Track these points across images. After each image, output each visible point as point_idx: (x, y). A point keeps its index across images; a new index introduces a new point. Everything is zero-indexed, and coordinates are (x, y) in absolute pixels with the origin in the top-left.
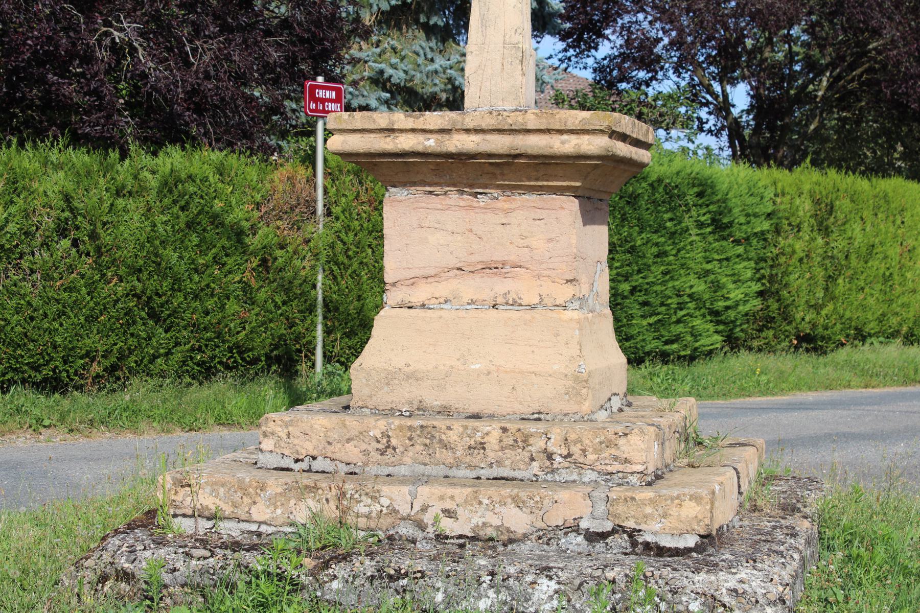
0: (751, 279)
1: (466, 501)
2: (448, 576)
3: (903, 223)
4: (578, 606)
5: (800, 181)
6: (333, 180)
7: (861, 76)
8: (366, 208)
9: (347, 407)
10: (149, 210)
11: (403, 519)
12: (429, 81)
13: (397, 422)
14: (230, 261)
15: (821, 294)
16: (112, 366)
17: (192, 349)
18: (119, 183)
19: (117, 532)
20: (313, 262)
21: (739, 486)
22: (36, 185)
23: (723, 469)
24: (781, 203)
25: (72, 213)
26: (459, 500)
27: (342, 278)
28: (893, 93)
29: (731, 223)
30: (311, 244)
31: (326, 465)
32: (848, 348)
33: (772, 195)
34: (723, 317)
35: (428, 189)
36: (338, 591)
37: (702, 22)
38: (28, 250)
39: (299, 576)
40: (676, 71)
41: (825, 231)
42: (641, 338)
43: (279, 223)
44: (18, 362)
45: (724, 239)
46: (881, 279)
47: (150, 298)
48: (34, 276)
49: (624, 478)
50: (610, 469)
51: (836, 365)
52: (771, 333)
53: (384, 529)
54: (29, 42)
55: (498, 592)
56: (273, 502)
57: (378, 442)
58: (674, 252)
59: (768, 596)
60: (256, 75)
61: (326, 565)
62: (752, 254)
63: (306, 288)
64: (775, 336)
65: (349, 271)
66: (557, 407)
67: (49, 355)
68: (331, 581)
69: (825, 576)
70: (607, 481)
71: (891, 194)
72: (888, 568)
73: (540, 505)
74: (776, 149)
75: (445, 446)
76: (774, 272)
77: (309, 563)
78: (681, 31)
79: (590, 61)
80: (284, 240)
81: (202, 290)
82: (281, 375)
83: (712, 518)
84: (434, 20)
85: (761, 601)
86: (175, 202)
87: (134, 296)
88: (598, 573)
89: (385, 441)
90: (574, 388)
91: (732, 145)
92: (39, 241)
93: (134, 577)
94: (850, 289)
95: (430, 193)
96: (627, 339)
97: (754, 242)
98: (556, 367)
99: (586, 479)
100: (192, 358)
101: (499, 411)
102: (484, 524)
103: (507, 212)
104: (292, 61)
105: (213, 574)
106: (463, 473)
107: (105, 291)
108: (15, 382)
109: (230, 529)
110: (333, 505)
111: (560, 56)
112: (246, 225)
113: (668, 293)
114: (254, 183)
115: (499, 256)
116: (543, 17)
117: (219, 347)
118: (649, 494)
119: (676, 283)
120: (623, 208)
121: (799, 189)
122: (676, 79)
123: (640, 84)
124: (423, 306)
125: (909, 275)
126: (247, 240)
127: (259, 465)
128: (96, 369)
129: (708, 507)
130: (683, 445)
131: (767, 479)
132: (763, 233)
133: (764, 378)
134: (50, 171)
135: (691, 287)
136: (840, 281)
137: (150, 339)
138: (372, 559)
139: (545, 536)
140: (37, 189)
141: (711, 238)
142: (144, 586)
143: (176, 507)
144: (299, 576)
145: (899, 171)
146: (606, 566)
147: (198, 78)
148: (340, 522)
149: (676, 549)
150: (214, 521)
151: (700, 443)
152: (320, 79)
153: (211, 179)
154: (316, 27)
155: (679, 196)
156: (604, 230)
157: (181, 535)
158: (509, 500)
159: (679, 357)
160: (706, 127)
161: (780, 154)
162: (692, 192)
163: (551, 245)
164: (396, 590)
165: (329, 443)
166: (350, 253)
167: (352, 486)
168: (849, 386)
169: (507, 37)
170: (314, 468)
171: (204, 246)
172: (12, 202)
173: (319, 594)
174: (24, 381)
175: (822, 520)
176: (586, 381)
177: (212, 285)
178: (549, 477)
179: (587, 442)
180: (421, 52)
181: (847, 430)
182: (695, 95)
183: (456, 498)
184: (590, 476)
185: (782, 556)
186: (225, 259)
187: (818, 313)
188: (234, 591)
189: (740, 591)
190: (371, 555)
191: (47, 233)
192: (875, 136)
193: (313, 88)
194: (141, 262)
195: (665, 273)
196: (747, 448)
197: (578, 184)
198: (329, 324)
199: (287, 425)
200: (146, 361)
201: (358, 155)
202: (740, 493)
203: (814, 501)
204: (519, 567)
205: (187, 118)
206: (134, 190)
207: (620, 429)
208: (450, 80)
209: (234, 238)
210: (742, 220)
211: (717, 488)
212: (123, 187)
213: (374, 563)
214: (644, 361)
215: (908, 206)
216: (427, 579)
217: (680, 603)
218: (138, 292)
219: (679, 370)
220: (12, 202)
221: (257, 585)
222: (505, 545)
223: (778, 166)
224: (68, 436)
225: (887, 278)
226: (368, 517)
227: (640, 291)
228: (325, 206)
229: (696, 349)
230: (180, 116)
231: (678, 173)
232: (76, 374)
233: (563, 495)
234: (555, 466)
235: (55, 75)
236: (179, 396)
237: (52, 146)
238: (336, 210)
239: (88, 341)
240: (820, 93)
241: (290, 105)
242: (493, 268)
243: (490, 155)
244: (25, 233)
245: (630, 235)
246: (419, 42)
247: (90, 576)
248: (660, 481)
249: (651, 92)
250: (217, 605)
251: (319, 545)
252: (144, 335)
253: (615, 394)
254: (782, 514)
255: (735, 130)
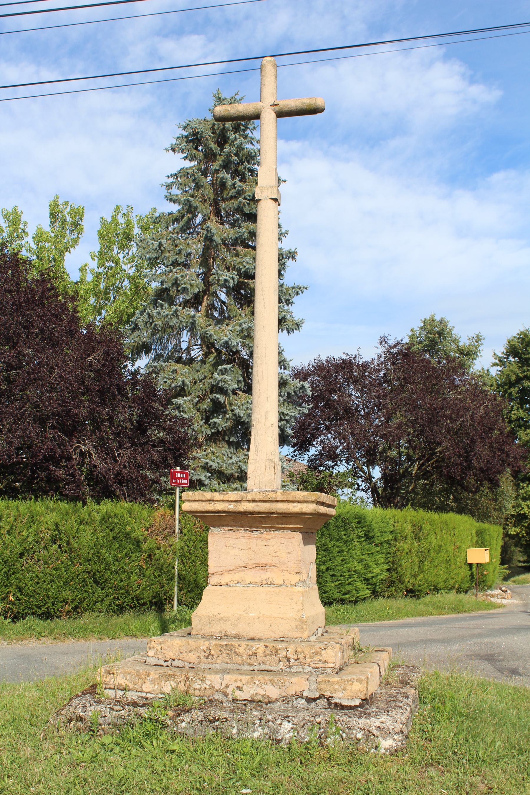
0: (384, 563)
1: (247, 682)
2: (239, 721)
3: (454, 534)
4: (302, 735)
5: (406, 515)
6: (183, 516)
7: (433, 464)
8: (199, 530)
9: (190, 634)
10: (95, 531)
11: (217, 691)
12: (229, 468)
13: (214, 642)
14: (133, 556)
15: (417, 570)
16: (75, 606)
17: (114, 598)
18: (81, 518)
19: (77, 696)
20: (173, 556)
21: (380, 673)
22: (42, 519)
23: (372, 664)
24: (397, 526)
25: (59, 532)
26: (244, 682)
27: (187, 563)
28: (448, 472)
29: (374, 536)
30: (173, 547)
31: (180, 664)
32: (430, 595)
33: (393, 522)
34: (371, 582)
35: (230, 528)
36: (185, 728)
37: (358, 439)
38: (37, 550)
39: (166, 720)
40: (347, 462)
41: (417, 538)
42: (331, 592)
43: (157, 537)
44: (30, 604)
45: (370, 543)
46: (445, 562)
47: (95, 573)
48: (40, 562)
49: (324, 670)
50: (317, 666)
51: (425, 604)
52: (393, 589)
53: (208, 696)
54: (42, 451)
55: (263, 729)
56: (153, 682)
57: (205, 652)
58: (347, 550)
59: (395, 729)
60: (148, 466)
61: (179, 715)
62: (384, 551)
63: (170, 568)
64: (396, 590)
65: (191, 560)
66: (292, 634)
67: (45, 601)
68: (181, 722)
69: (422, 718)
70: (316, 672)
71: (448, 521)
72: (452, 713)
73: (283, 684)
74: (394, 498)
75: (237, 654)
76: (394, 559)
77: (171, 713)
78: (348, 443)
79: (306, 457)
80: (160, 545)
81: (120, 569)
82: (157, 611)
83: (367, 690)
84: (232, 439)
85: (391, 732)
86: (108, 527)
87: (87, 572)
88: (312, 719)
89: (208, 652)
90: (300, 625)
91: (373, 496)
92: (43, 545)
93: (85, 720)
94: (430, 567)
95: (231, 530)
96: (325, 593)
97: (385, 545)
98: (291, 615)
99: (306, 671)
100: (114, 603)
101: (263, 636)
102: (256, 694)
103: (267, 540)
104: (165, 459)
105: (124, 719)
106: (246, 667)
107: (73, 570)
108: (29, 614)
109: (132, 696)
110: (182, 684)
111: (292, 454)
112: (141, 538)
113: (344, 570)
114: (145, 518)
115: (263, 561)
116: (284, 437)
117: (127, 597)
118: (336, 679)
119: (348, 565)
120: (322, 529)
121: (405, 519)
122: (347, 465)
123: (330, 468)
124: (227, 585)
125: (458, 559)
126: (142, 545)
127: (147, 663)
128: (67, 608)
129: (365, 685)
130: (353, 652)
131: (394, 667)
132: (389, 540)
133: (391, 611)
134: (49, 512)
135: (355, 567)
136: (426, 563)
137: (94, 593)
138: (202, 712)
139: (286, 700)
140: (43, 521)
141: (364, 544)
142: (91, 725)
143: (107, 684)
144: (166, 720)
145: (452, 510)
146: (316, 715)
147: (120, 468)
148: (186, 693)
149: (350, 706)
150: (124, 692)
151: (361, 650)
152: (178, 468)
153: (125, 516)
154: (177, 443)
155: (348, 523)
156: (314, 547)
157: (108, 698)
158: (269, 682)
159: (350, 601)
160: (361, 488)
161: (396, 501)
162: (354, 521)
163: (288, 556)
164: (213, 728)
165: (181, 653)
166: (191, 552)
167: (192, 675)
168: (431, 615)
169: (268, 456)
170: (174, 665)
171: (121, 548)
172: (31, 527)
173: (175, 729)
174: (33, 614)
175: (421, 688)
176: (306, 622)
177: (125, 567)
178: (288, 670)
179: (306, 652)
180: (226, 454)
181: (431, 637)
182: (355, 473)
183: (243, 681)
184: (308, 669)
185: (402, 709)
186: (131, 554)
187: (416, 579)
188: (134, 728)
189: (382, 728)
190: (201, 709)
191: (47, 542)
192: (440, 492)
193: (175, 473)
194: (91, 556)
195: (342, 561)
196: (383, 653)
197: (301, 526)
198: (180, 586)
199: (160, 643)
200: (92, 604)
201: (196, 512)
202: (381, 676)
203: (416, 678)
204: (273, 716)
205: (115, 487)
206: (89, 521)
207: (322, 646)
208: (239, 467)
209: (135, 544)
210: (379, 534)
211: (370, 675)
212: (83, 520)
213: (202, 714)
214: (332, 603)
215: (456, 526)
216: (228, 722)
217: (353, 734)
218: (89, 570)
219: (350, 608)
220: (31, 527)
221: (145, 725)
222: (267, 704)
223: (395, 508)
224: (53, 641)
225: (448, 561)
226: (200, 690)
227: (331, 569)
228: (179, 529)
229: (358, 597)
230: (112, 486)
231: (348, 512)
232: (58, 610)
233: (295, 679)
234: (291, 664)
235: (53, 466)
236: (107, 622)
237: (51, 500)
238: (185, 531)
239: (64, 594)
240: (414, 472)
241: (163, 479)
242: (260, 566)
243: (259, 513)
244: (36, 542)
245: (326, 542)
246: (225, 449)
247: (64, 719)
248: (342, 671)
249: (335, 471)
250: (125, 735)
251: (176, 704)
252: (91, 591)
253: (319, 627)
254: (400, 685)
255: (374, 490)
